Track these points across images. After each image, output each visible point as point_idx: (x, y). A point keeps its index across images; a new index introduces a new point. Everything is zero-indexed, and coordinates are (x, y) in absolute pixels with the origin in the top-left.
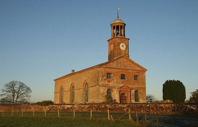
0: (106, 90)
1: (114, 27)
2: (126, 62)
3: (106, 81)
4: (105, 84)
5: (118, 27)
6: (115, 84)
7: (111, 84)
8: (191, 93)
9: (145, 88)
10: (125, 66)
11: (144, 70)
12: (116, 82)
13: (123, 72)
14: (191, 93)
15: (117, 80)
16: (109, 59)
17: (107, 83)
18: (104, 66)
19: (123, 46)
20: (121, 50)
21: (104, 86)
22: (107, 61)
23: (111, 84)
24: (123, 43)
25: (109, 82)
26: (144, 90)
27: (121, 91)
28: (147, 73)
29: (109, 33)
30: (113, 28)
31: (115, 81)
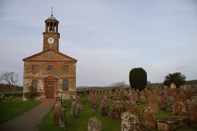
0: (31, 82)
1: (48, 23)
2: (53, 54)
3: (31, 73)
4: (30, 76)
5: (51, 23)
6: (41, 76)
7: (36, 76)
8: (52, 15)
9: (75, 78)
10: (53, 58)
11: (75, 61)
12: (42, 74)
13: (51, 63)
14: (52, 15)
15: (43, 71)
16: (44, 48)
17: (32, 75)
18: (29, 60)
19: (51, 40)
20: (49, 44)
21: (29, 78)
22: (41, 50)
23: (36, 76)
24: (51, 37)
25: (34, 73)
26: (74, 79)
27: (46, 81)
28: (77, 64)
29: (43, 27)
30: (47, 24)
31: (41, 72)
